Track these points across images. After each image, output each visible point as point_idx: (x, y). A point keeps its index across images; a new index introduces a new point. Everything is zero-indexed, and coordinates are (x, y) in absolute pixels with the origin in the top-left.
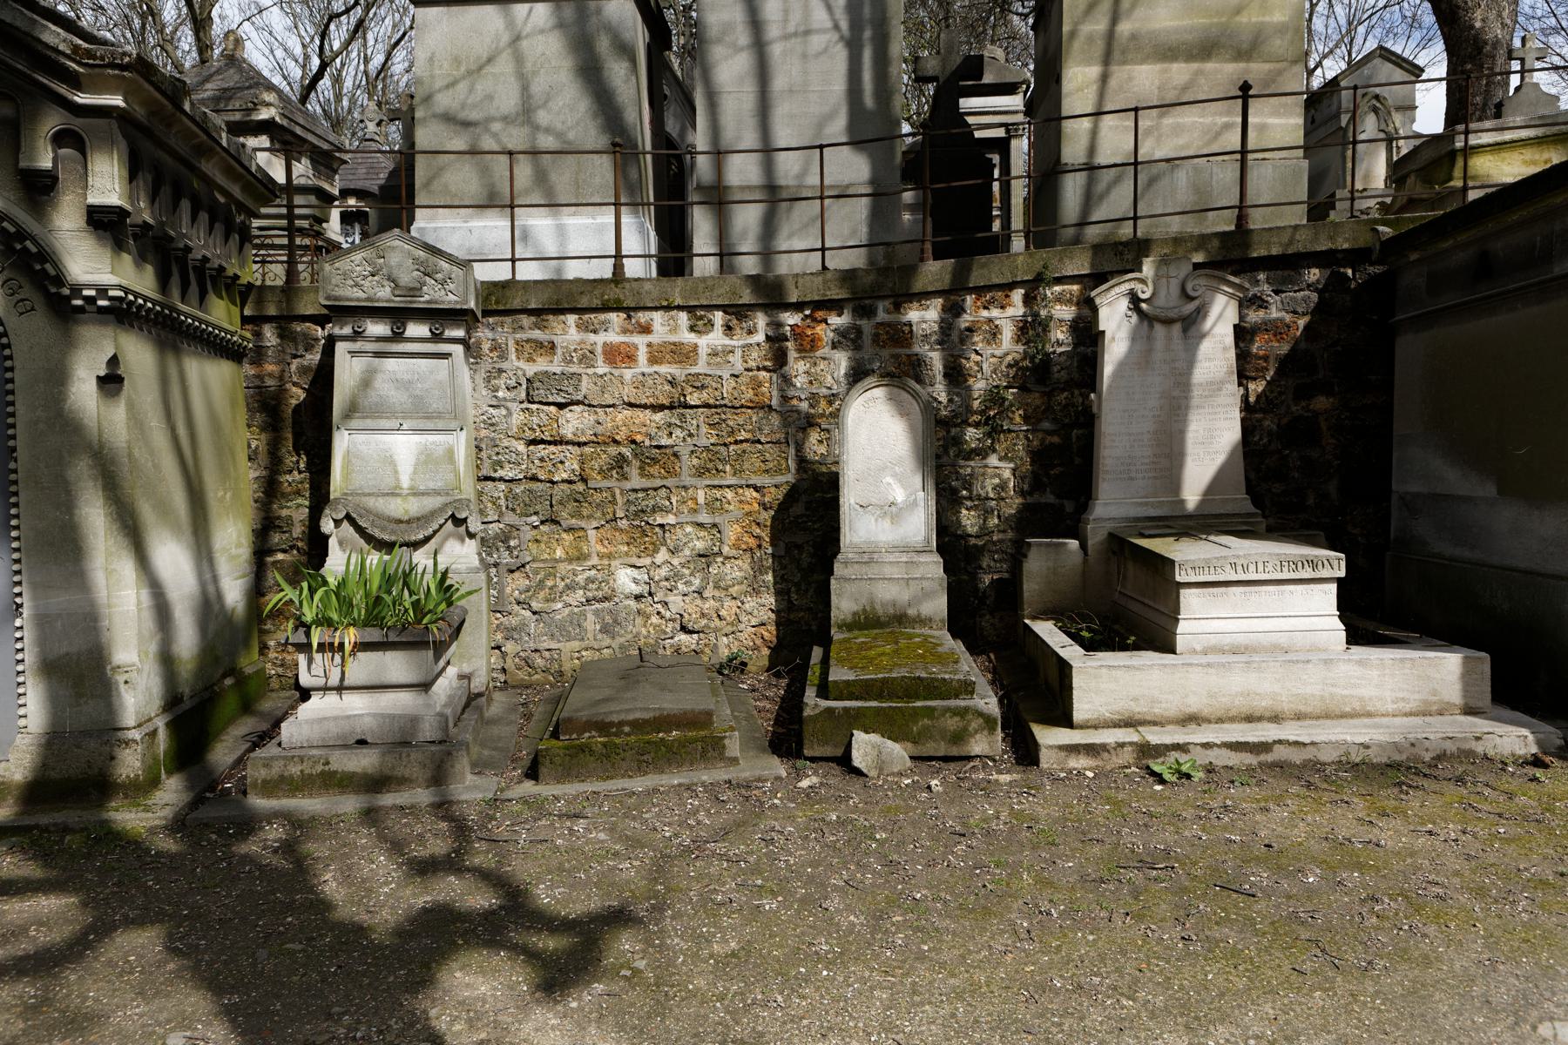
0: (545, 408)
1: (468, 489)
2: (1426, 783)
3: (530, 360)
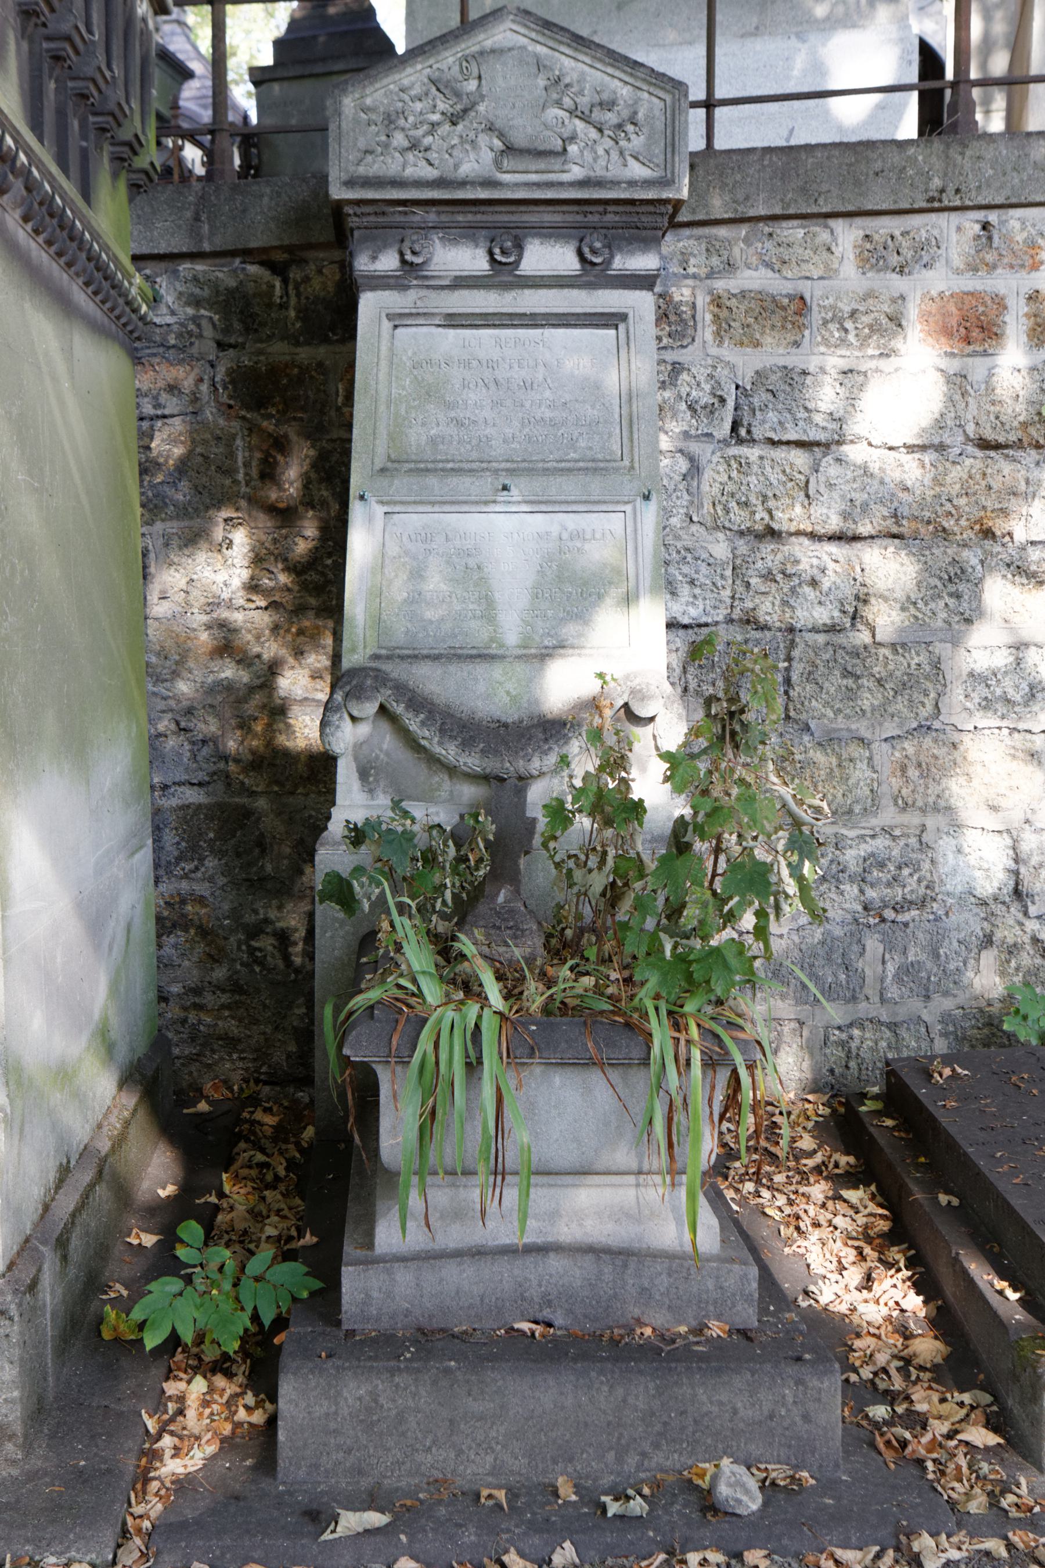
2: (16, 1137)
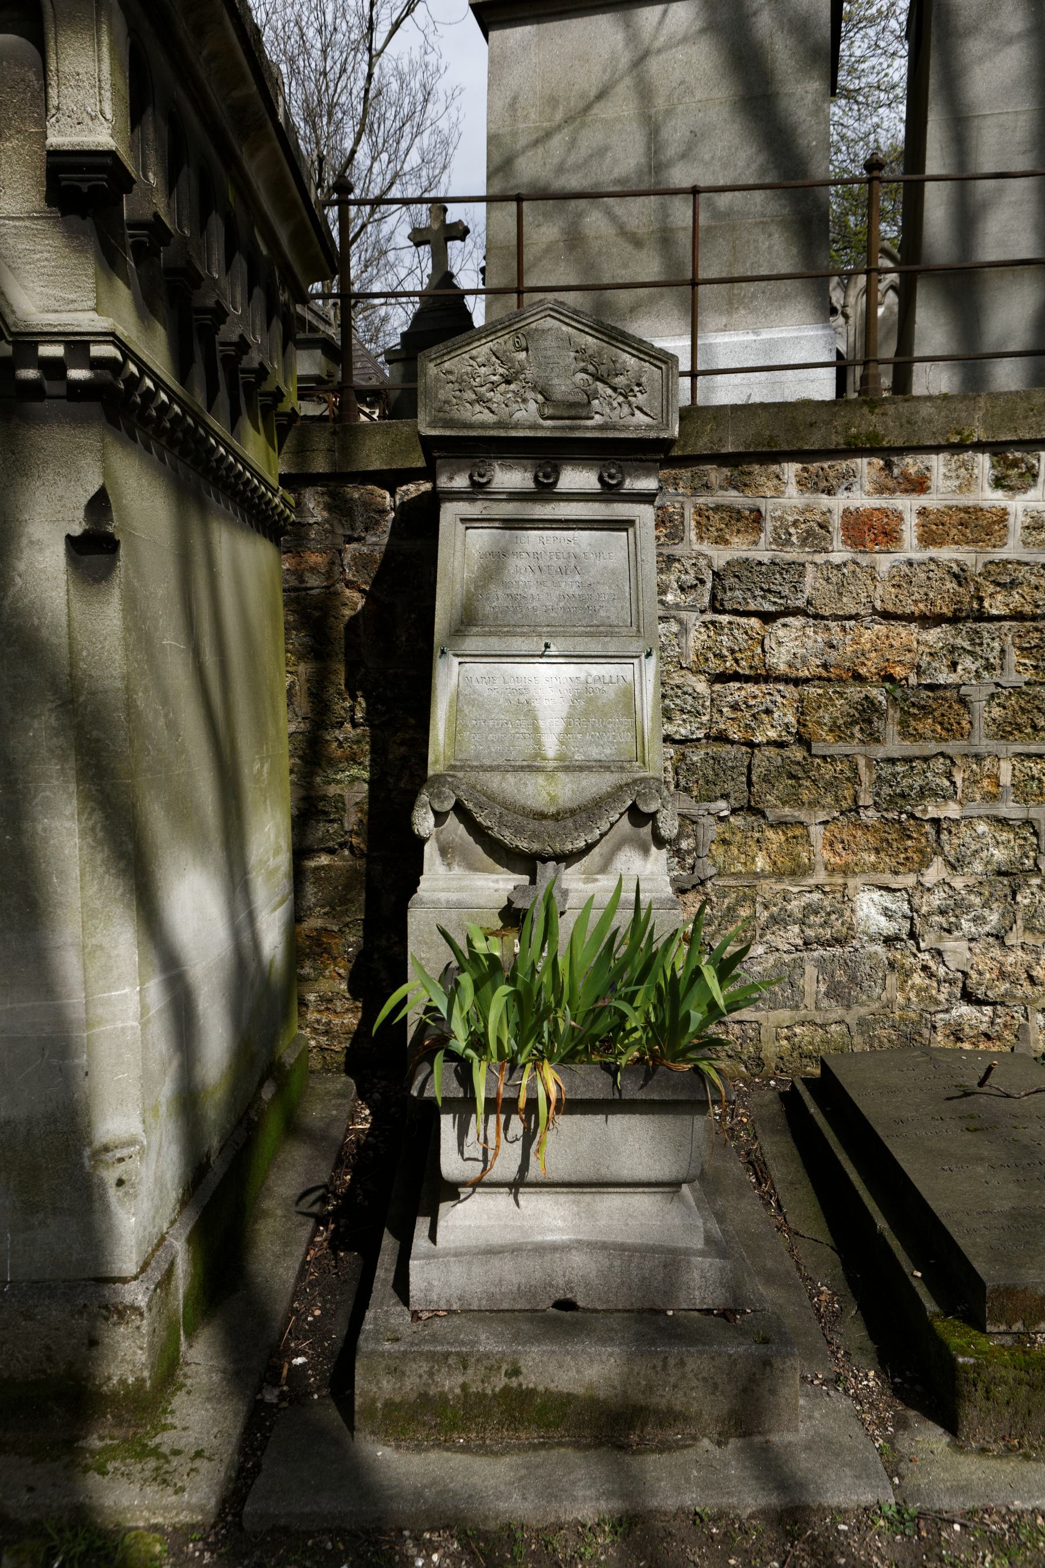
0: (743, 620)
1: (659, 760)
3: (721, 540)
